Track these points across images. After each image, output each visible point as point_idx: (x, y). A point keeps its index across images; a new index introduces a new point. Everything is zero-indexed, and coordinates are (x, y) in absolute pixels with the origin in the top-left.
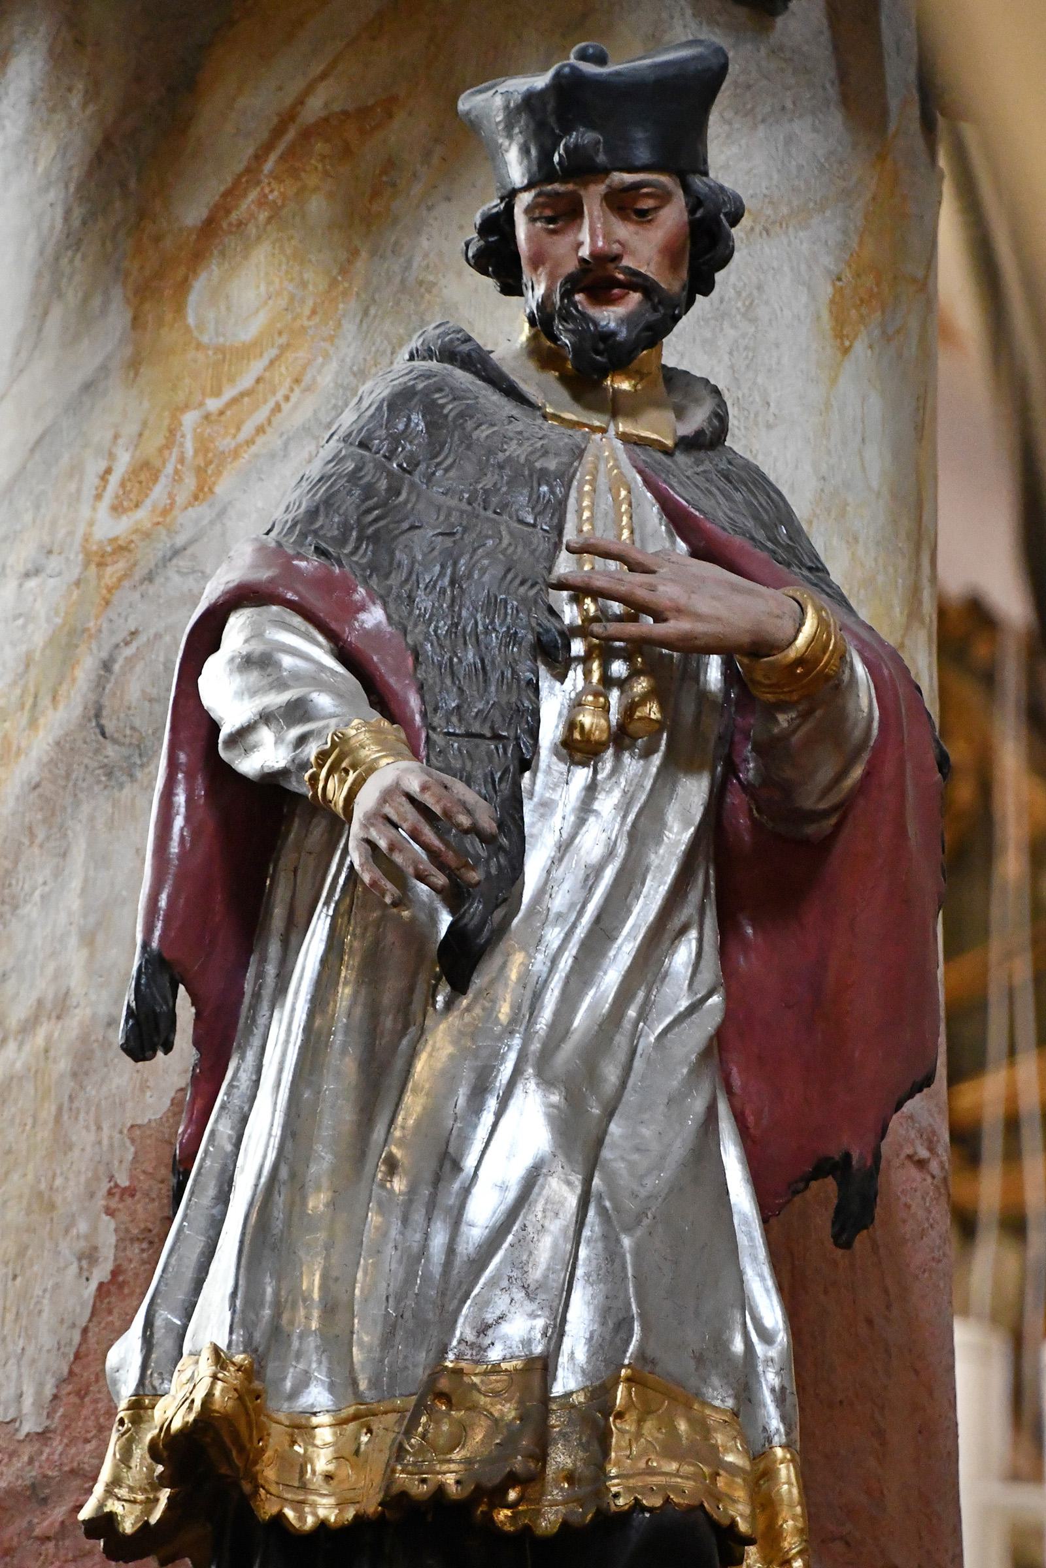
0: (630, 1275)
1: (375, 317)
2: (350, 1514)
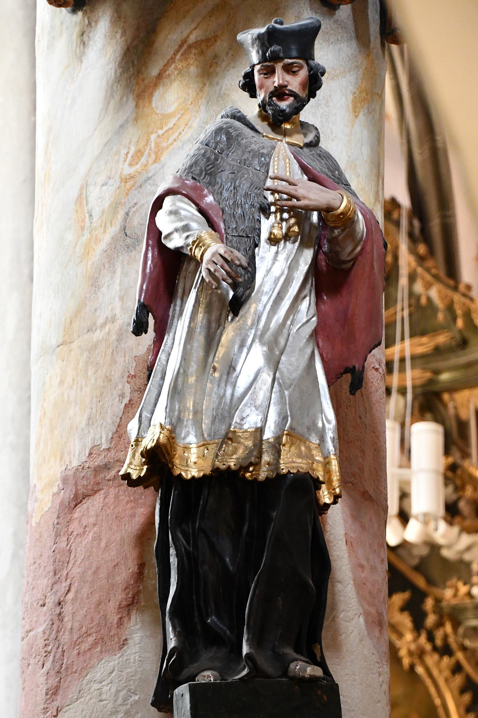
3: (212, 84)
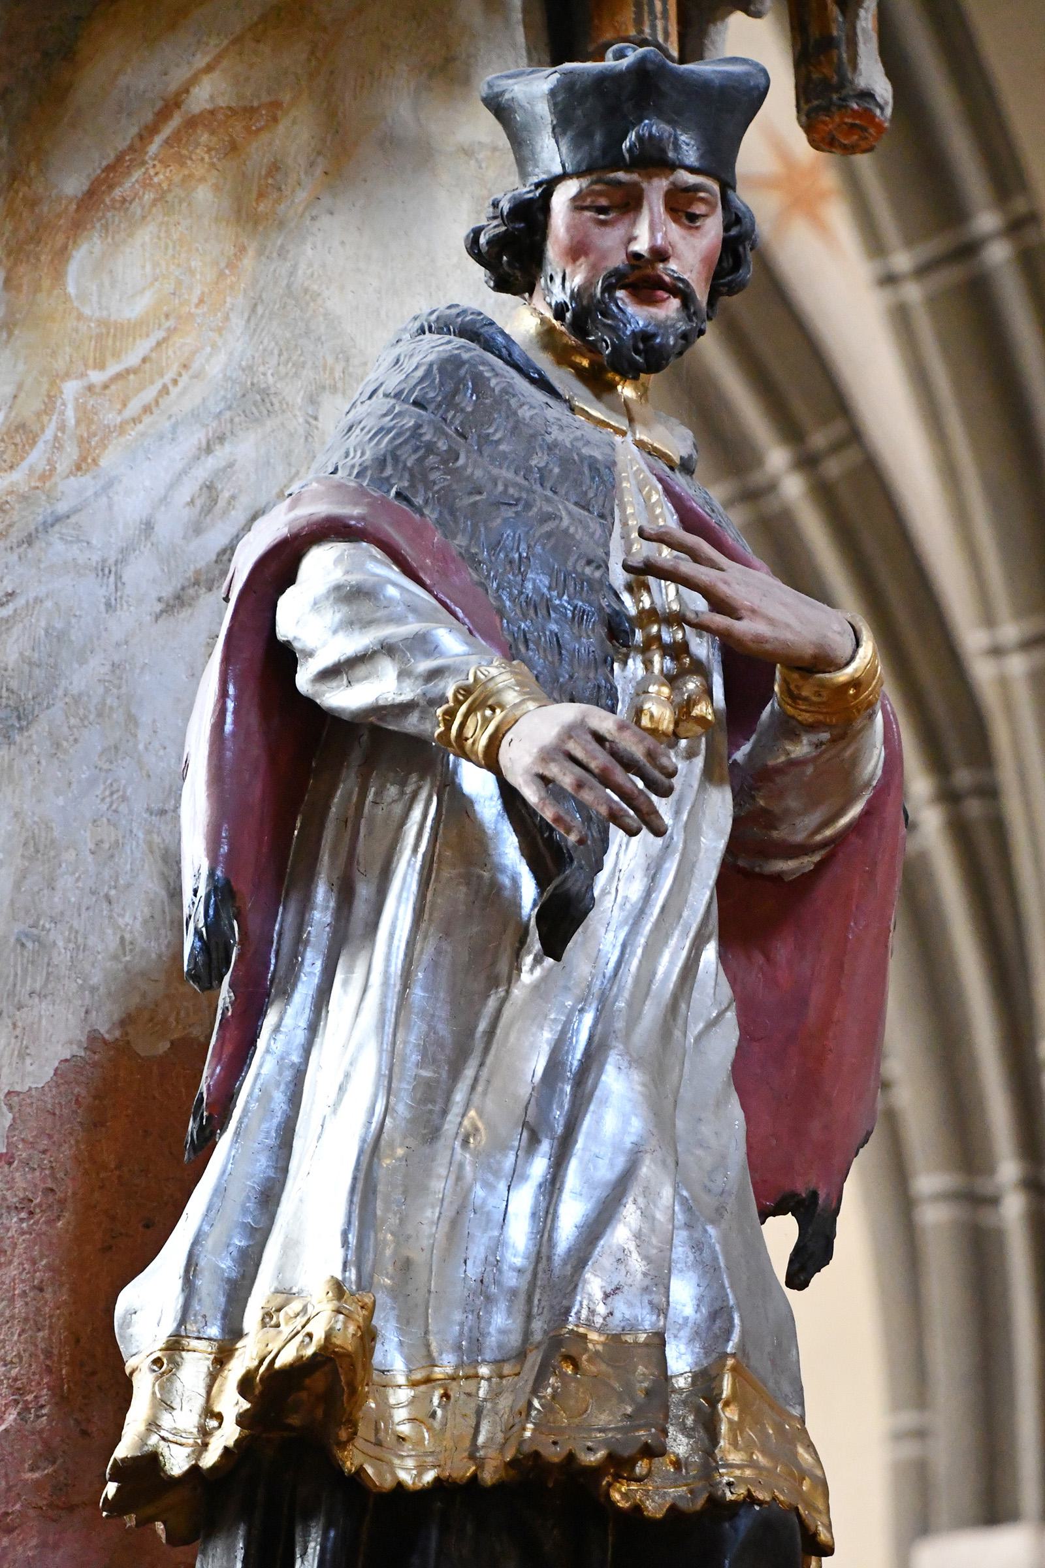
0: (722, 1265)
1: (262, 316)
2: (429, 1477)
3: (267, 253)
